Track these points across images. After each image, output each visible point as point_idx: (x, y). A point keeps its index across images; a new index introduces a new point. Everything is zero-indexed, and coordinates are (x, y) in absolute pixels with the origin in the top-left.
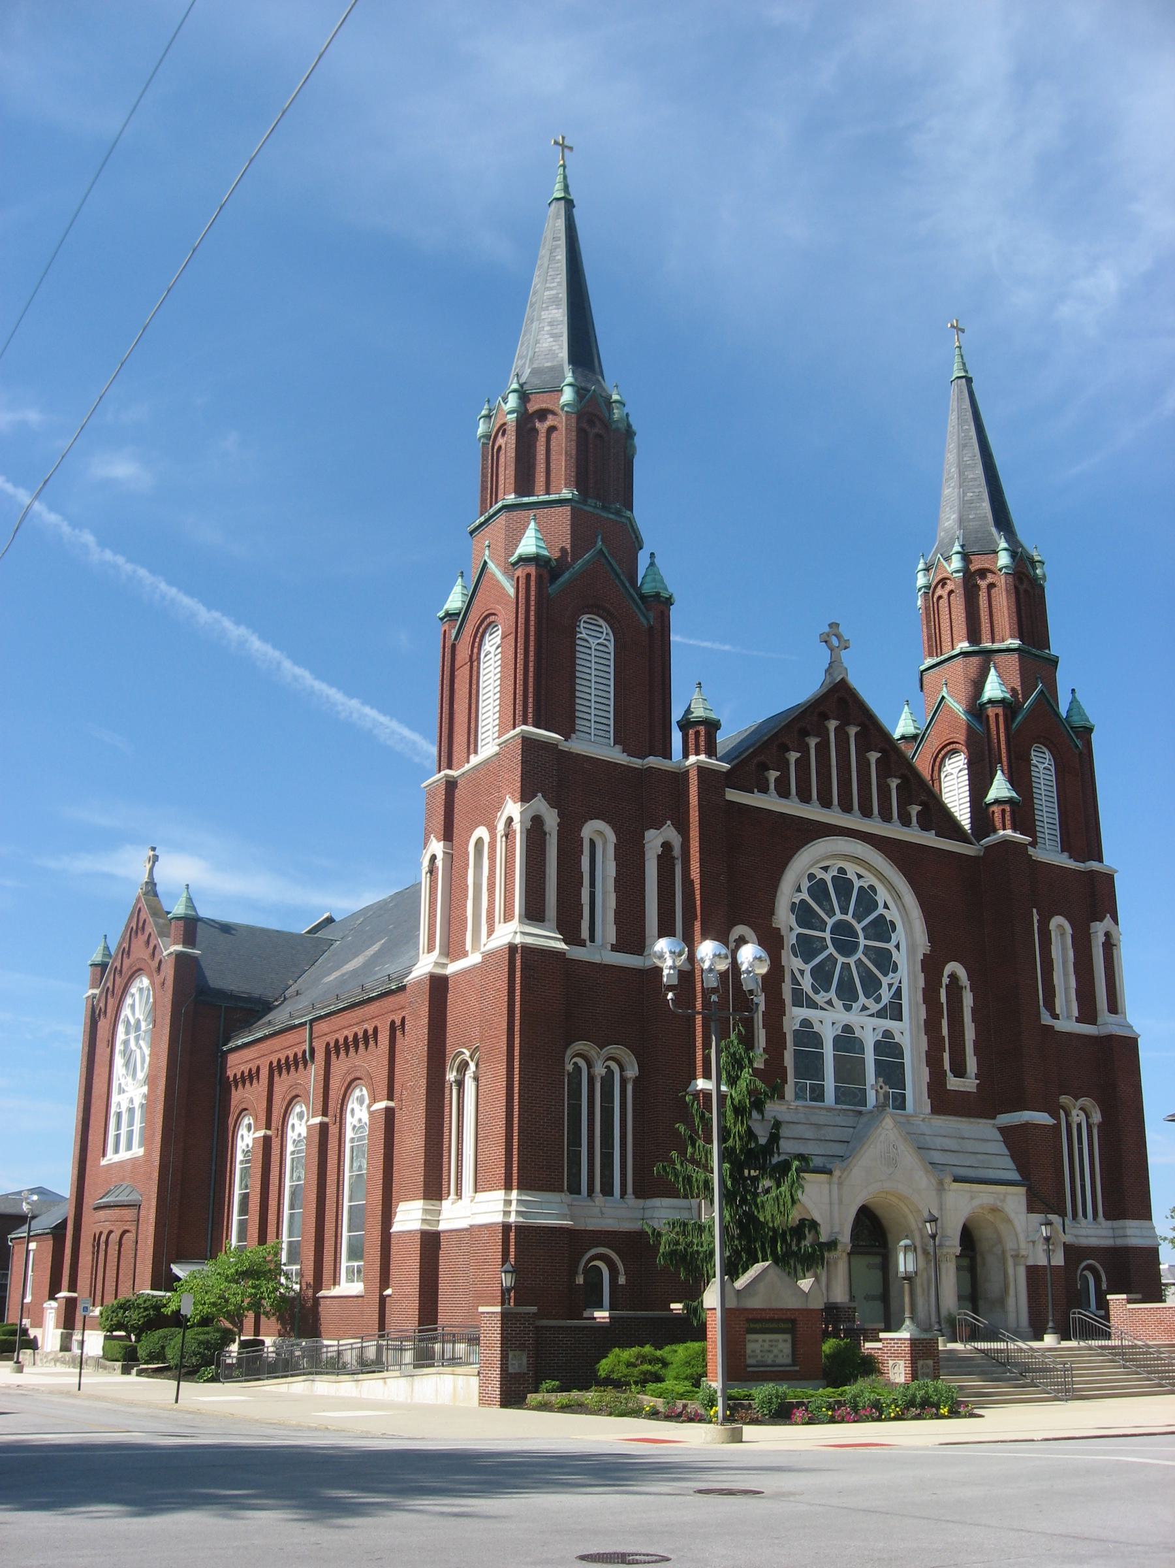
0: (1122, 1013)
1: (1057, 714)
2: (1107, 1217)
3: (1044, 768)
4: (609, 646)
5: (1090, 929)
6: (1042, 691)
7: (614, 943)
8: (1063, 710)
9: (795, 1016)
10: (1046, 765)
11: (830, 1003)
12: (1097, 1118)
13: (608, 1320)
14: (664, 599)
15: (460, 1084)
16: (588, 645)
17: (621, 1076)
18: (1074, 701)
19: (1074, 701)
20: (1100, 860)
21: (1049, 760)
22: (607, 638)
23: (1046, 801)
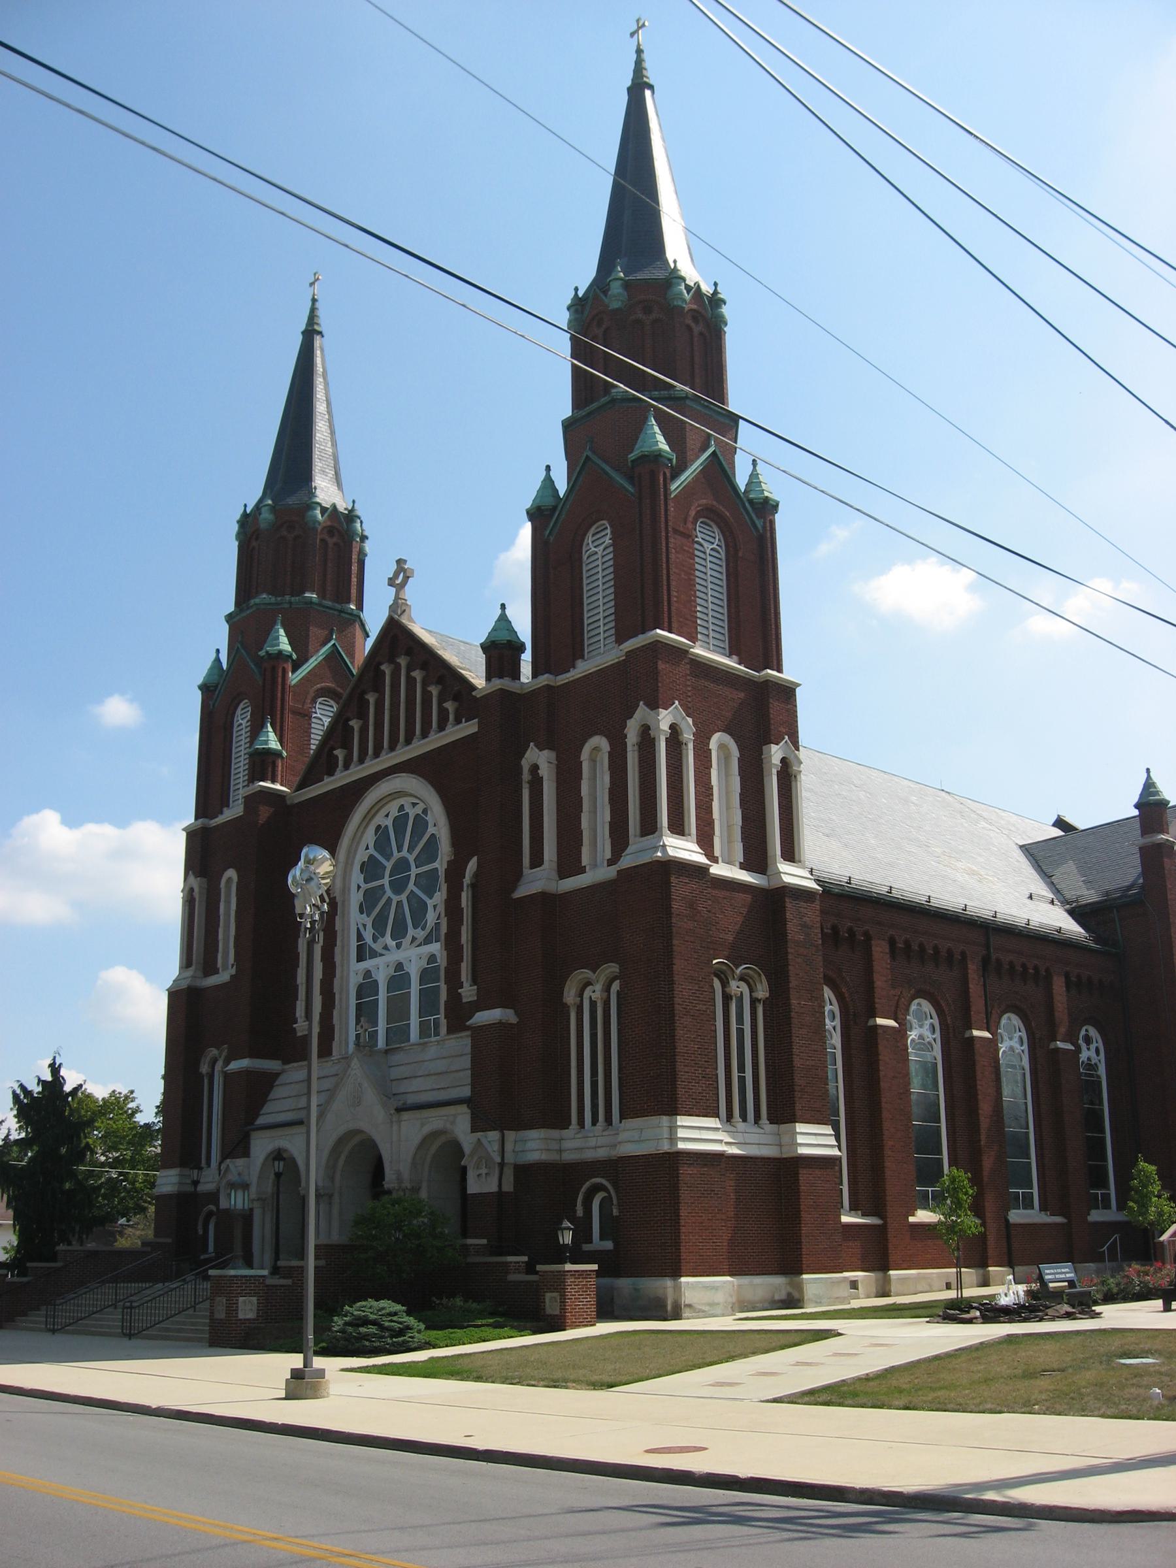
0: (800, 862)
1: (734, 488)
2: (773, 1120)
3: (712, 549)
4: (720, 550)
5: (762, 754)
6: (714, 453)
7: (742, 861)
8: (741, 481)
9: (352, 972)
10: (714, 546)
11: (386, 948)
12: (762, 992)
13: (561, 1242)
14: (760, 506)
15: (211, 1076)
16: (703, 550)
17: (724, 992)
18: (754, 475)
19: (754, 475)
20: (780, 670)
21: (719, 540)
22: (719, 544)
23: (711, 582)
